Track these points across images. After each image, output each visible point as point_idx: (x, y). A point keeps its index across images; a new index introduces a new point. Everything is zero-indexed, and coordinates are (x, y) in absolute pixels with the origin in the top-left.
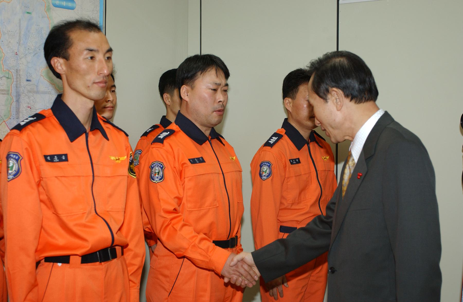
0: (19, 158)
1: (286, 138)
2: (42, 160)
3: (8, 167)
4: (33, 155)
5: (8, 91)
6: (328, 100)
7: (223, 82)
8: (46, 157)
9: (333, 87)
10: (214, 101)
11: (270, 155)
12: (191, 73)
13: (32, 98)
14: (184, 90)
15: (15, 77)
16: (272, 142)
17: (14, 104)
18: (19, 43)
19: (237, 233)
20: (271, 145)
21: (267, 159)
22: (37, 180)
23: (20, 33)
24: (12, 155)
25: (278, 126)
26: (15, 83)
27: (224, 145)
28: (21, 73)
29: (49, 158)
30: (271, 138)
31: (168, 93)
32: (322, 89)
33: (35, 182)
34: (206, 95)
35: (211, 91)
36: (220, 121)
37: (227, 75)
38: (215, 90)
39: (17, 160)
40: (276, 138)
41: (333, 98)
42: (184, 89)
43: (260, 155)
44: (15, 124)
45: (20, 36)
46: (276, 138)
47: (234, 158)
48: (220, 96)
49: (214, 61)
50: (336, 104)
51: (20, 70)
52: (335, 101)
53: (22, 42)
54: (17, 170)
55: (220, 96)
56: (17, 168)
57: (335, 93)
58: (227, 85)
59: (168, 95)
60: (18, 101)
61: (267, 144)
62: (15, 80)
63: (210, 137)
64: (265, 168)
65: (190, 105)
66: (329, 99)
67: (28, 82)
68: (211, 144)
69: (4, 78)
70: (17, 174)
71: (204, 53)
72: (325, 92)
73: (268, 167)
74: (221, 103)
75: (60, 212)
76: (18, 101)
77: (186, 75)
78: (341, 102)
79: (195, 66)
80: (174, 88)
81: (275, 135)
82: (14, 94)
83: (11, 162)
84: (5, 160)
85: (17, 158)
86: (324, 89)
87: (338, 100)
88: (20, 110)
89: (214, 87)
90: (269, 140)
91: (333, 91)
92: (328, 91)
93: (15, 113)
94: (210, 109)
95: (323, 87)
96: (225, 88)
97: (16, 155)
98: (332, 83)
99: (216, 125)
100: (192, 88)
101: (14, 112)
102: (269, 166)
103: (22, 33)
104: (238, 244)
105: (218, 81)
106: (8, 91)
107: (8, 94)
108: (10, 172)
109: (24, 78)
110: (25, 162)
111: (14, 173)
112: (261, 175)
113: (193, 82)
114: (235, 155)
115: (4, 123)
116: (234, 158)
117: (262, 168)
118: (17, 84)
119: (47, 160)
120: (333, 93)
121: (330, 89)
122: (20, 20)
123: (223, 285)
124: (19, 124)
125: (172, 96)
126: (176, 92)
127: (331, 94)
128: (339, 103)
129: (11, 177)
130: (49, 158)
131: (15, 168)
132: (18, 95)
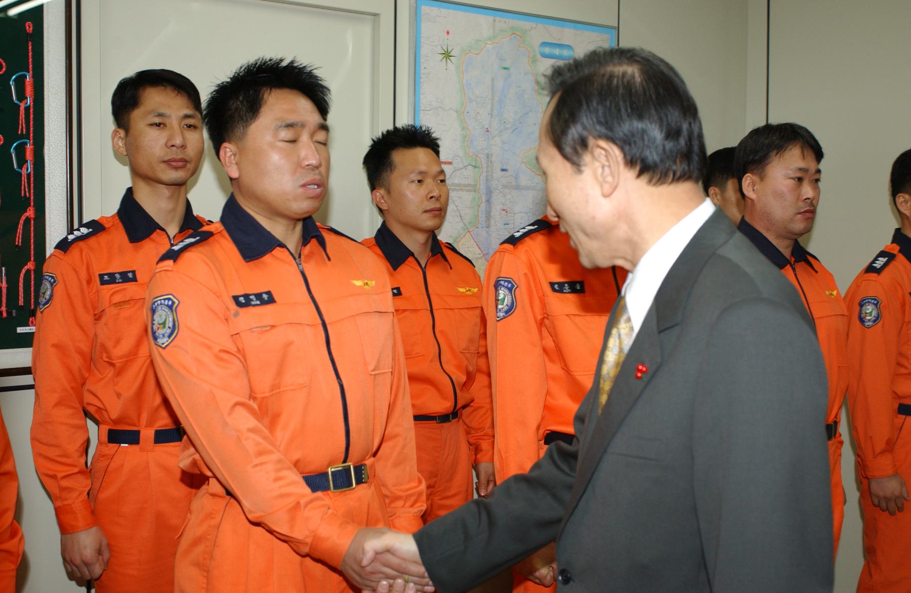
0: (513, 286)
1: (901, 258)
2: (547, 289)
3: (497, 300)
4: (534, 280)
5: (475, 185)
6: (583, 168)
7: (811, 165)
8: (236, 298)
9: (600, 136)
10: (798, 199)
11: (876, 286)
12: (760, 154)
13: (509, 196)
14: (748, 182)
15: (485, 165)
16: (878, 265)
17: (483, 205)
18: (491, 115)
19: (836, 417)
20: (878, 271)
21: (871, 293)
22: (539, 317)
23: (493, 99)
24: (502, 283)
25: (885, 240)
26: (485, 174)
27: (817, 272)
28: (494, 159)
29: (242, 299)
30: (876, 259)
31: (716, 186)
32: (570, 137)
33: (536, 322)
34: (785, 189)
35: (792, 181)
36: (808, 230)
37: (818, 154)
38: (800, 180)
39: (510, 290)
40: (885, 260)
41: (597, 164)
42: (748, 180)
43: (858, 287)
44: (507, 236)
45: (492, 104)
46: (885, 260)
47: (835, 293)
48: (807, 191)
49: (798, 133)
50: (600, 179)
51: (492, 155)
52: (600, 171)
53: (495, 112)
54: (509, 304)
55: (807, 191)
56: (510, 301)
57: (603, 152)
58: (819, 171)
59: (717, 190)
60: (488, 201)
61: (870, 269)
62: (485, 170)
63: (793, 259)
64: (869, 308)
65: (759, 206)
66: (585, 165)
67: (504, 173)
68: (794, 269)
69: (470, 167)
70: (510, 310)
71: (775, 120)
72: (579, 149)
73: (874, 307)
74: (808, 201)
75: (573, 367)
76: (488, 201)
77: (751, 157)
78: (613, 176)
79: (767, 142)
80: (727, 179)
81: (882, 254)
82: (482, 188)
83: (502, 293)
84: (492, 289)
85: (170, 303)
86: (576, 136)
87: (607, 169)
88: (492, 214)
89: (799, 175)
90: (873, 262)
91: (599, 146)
92: (583, 143)
93: (484, 219)
94: (791, 212)
95: (574, 132)
96: (816, 177)
97: (509, 282)
98: (598, 127)
99: (801, 234)
100: (762, 178)
101: (482, 218)
102: (876, 305)
103: (496, 99)
104: (838, 435)
105: (802, 165)
106: (475, 185)
107: (475, 191)
108: (500, 307)
109: (497, 167)
110: (522, 293)
111: (506, 308)
112: (862, 320)
113: (247, 126)
114: (836, 288)
115: (468, 235)
116: (835, 293)
117: (864, 308)
118: (487, 176)
119: (554, 290)
120: (598, 151)
121: (591, 142)
122: (493, 79)
123: (569, 585)
124: (513, 236)
125: (723, 190)
126: (731, 185)
127: (592, 153)
128: (609, 179)
129: (501, 314)
130: (242, 299)
131: (508, 301)
132: (489, 192)
